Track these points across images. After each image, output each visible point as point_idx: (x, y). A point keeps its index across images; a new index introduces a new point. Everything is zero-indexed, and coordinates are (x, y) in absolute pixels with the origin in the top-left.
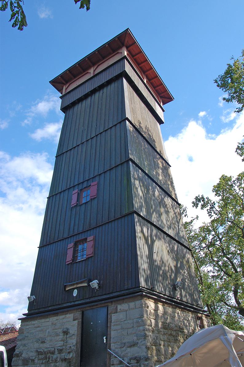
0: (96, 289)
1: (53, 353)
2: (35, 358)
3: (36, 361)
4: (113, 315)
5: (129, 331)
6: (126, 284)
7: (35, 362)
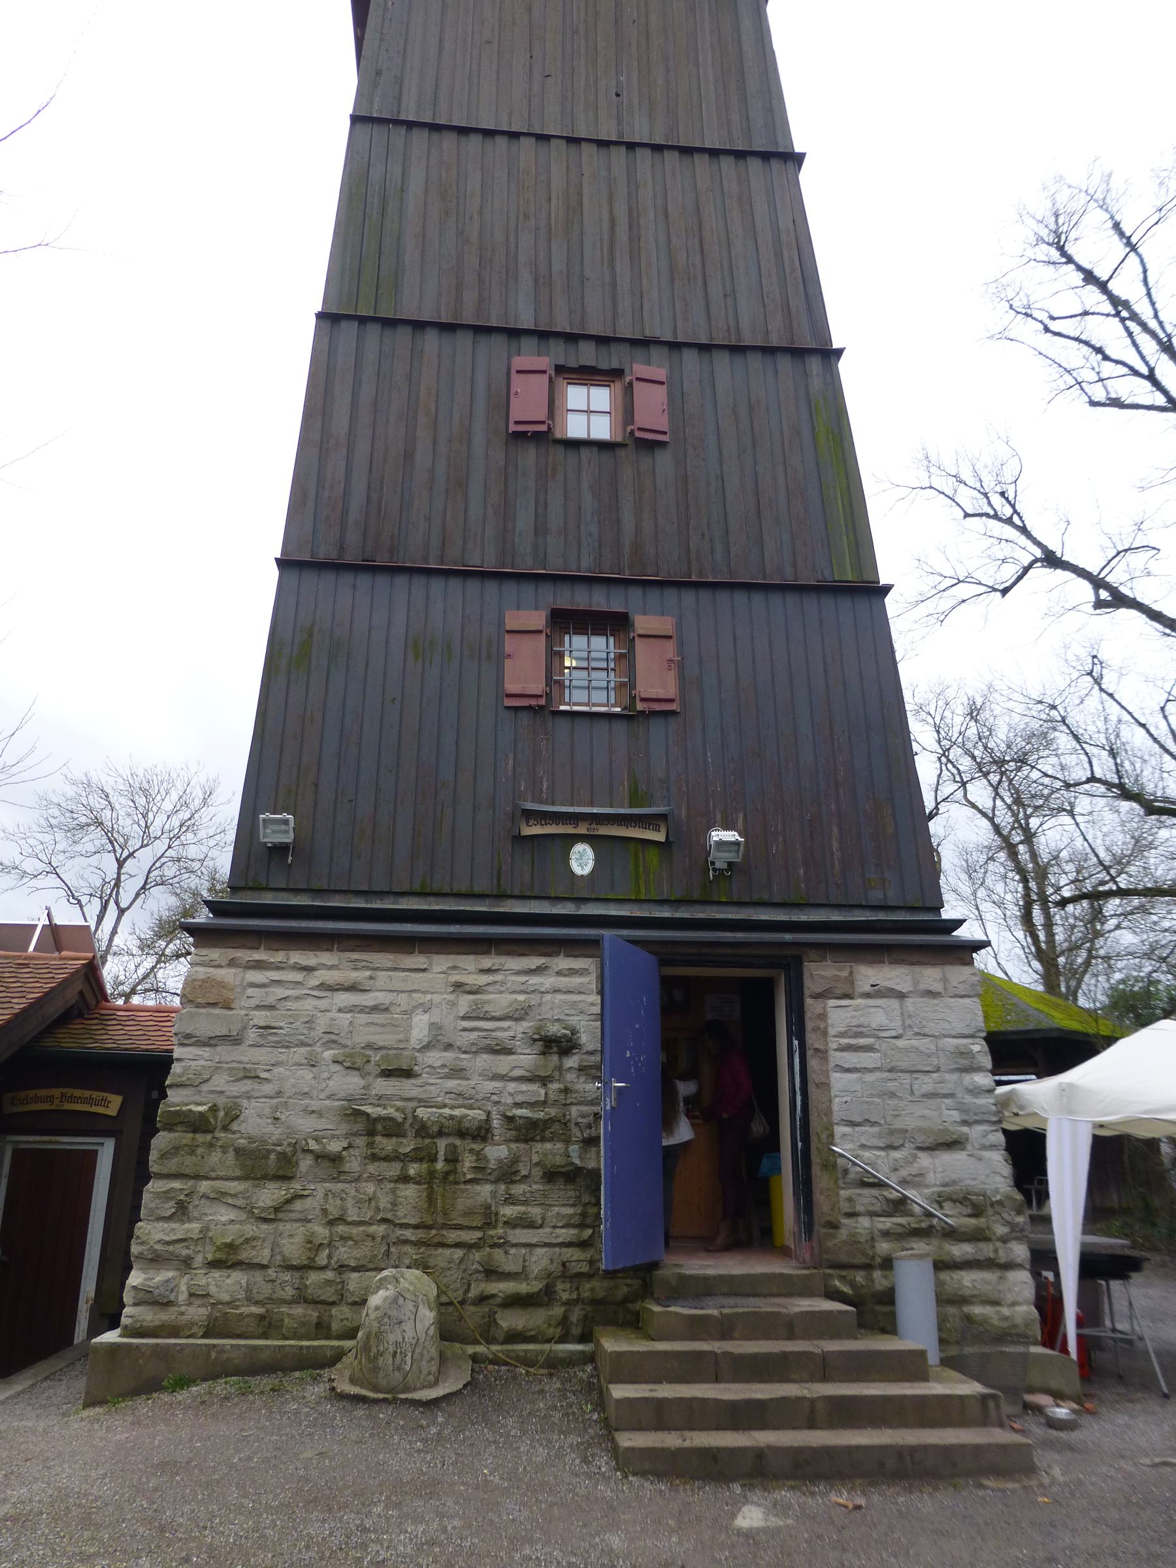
0: (715, 870)
1: (482, 1133)
2: (345, 1149)
3: (353, 1164)
4: (832, 1003)
5: (919, 1081)
6: (497, 1138)
7: (347, 1167)
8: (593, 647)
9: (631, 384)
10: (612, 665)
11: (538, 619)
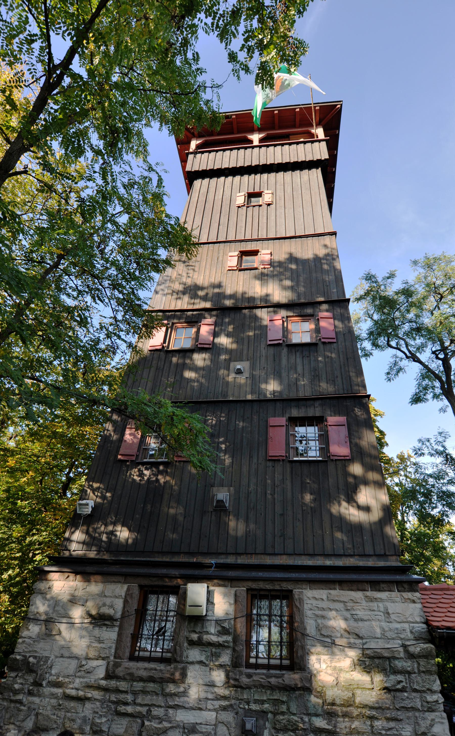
8: (308, 431)
9: (318, 319)
10: (317, 439)
11: (283, 421)
